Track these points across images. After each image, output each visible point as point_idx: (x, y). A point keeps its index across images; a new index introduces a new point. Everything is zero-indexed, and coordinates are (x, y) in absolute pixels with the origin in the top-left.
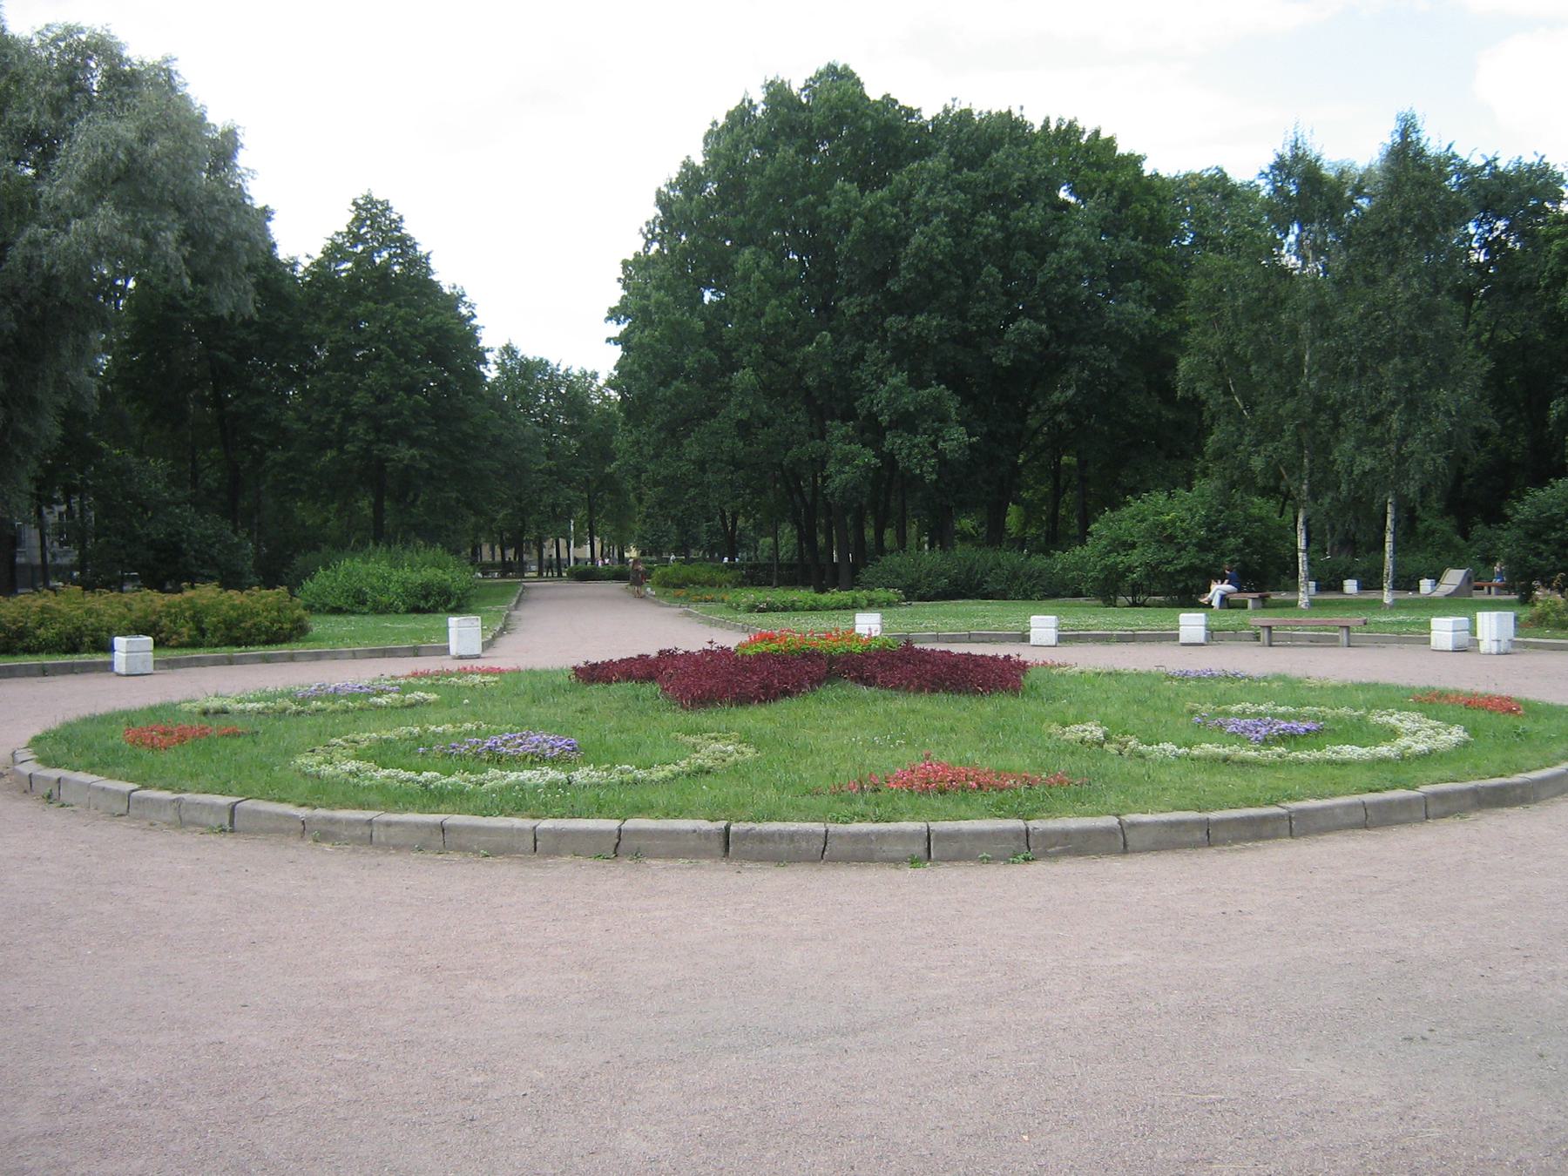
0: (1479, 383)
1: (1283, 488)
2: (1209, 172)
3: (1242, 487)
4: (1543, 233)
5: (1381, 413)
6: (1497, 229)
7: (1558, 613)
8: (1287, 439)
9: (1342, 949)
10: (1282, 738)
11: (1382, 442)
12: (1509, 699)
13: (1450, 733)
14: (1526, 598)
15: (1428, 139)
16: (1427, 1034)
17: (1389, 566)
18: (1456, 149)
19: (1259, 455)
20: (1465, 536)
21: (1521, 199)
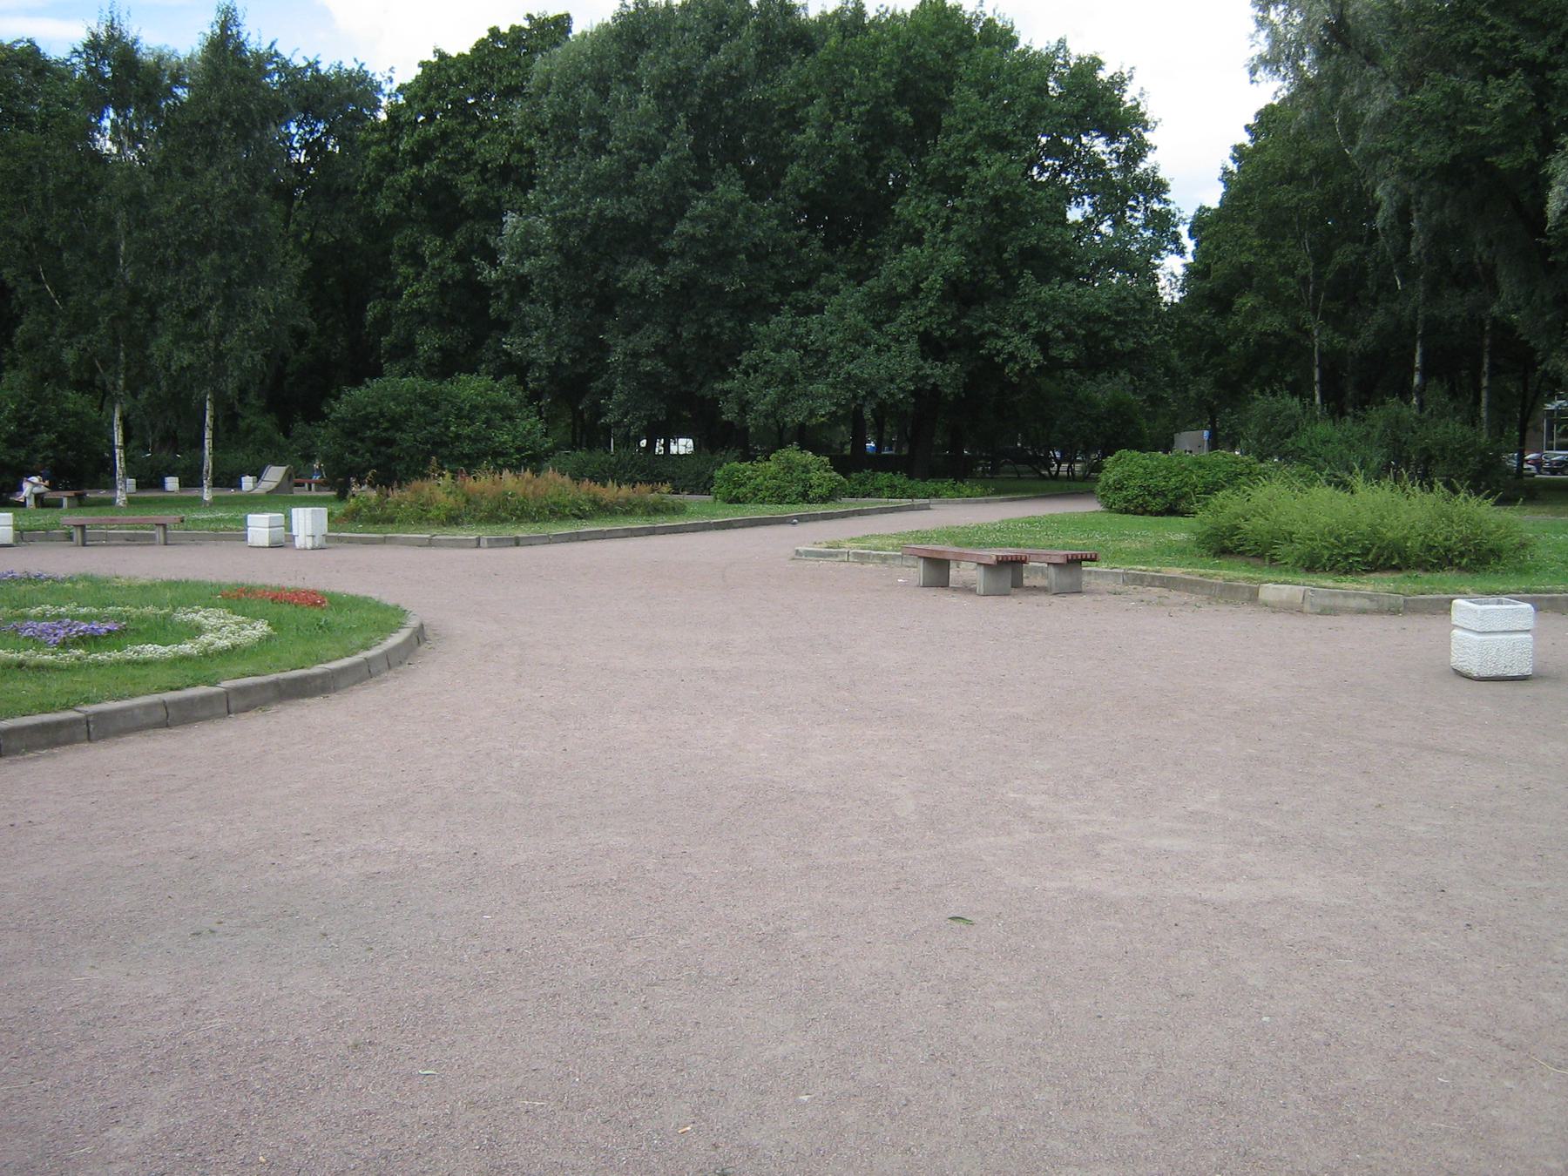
0: (296, 282)
1: (98, 383)
2: (21, 45)
3: (54, 380)
4: (361, 138)
5: (199, 308)
6: (318, 131)
7: (370, 508)
8: (102, 331)
9: (135, 851)
10: (86, 640)
11: (200, 338)
12: (314, 593)
13: (254, 628)
14: (342, 496)
15: (249, 34)
16: (215, 927)
17: (208, 463)
18: (279, 47)
19: (72, 348)
20: (287, 435)
21: (340, 104)
